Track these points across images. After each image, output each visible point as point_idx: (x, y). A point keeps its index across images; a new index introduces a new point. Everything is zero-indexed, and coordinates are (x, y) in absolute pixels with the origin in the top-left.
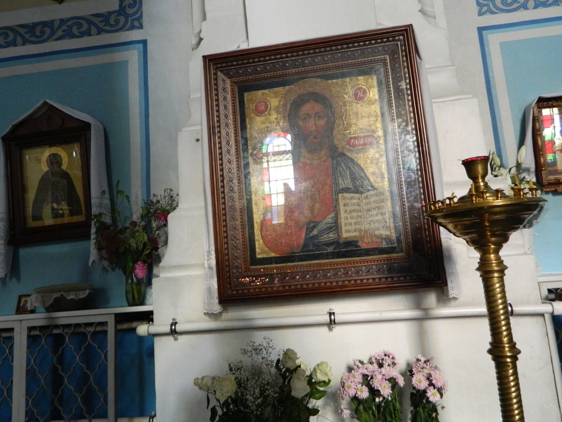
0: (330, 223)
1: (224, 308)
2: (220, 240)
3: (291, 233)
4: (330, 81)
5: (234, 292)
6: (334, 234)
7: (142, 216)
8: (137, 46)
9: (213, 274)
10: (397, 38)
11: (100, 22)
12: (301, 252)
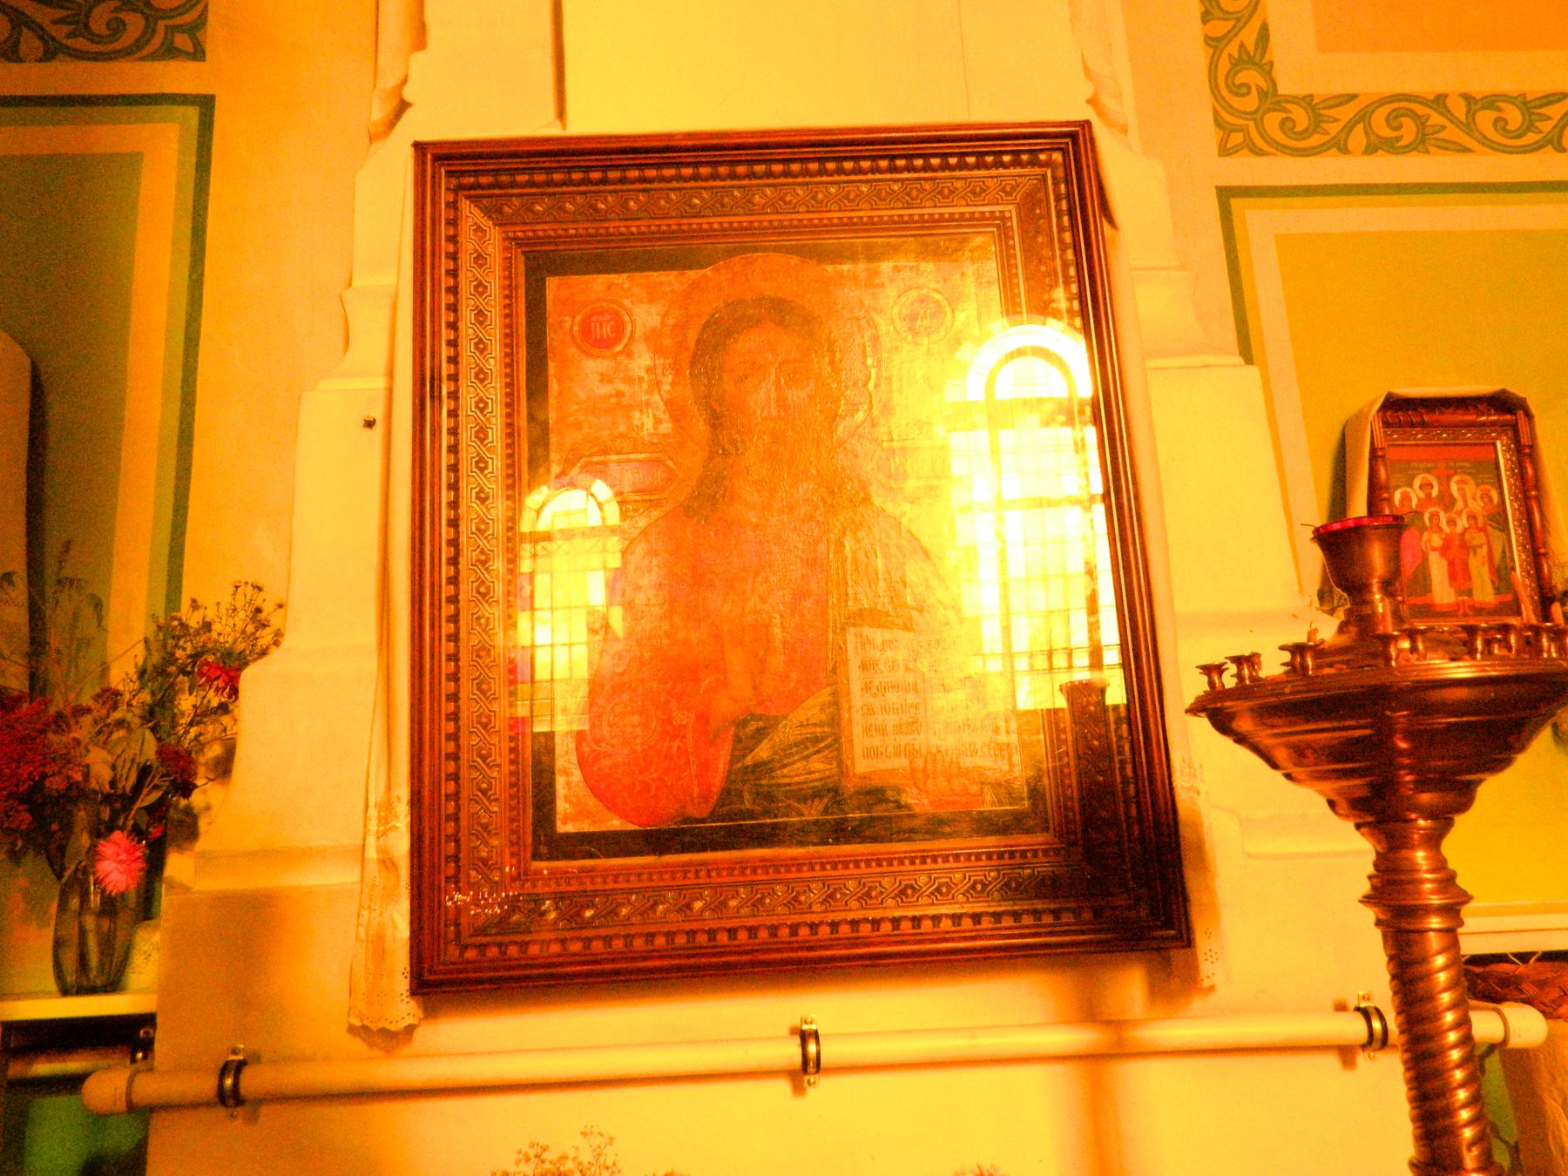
0: (815, 725)
1: (425, 1009)
2: (432, 765)
3: (682, 751)
4: (829, 268)
5: (471, 954)
6: (828, 760)
7: (142, 673)
8: (180, 110)
9: (397, 885)
10: (1043, 157)
11: (55, 22)
12: (713, 816)
